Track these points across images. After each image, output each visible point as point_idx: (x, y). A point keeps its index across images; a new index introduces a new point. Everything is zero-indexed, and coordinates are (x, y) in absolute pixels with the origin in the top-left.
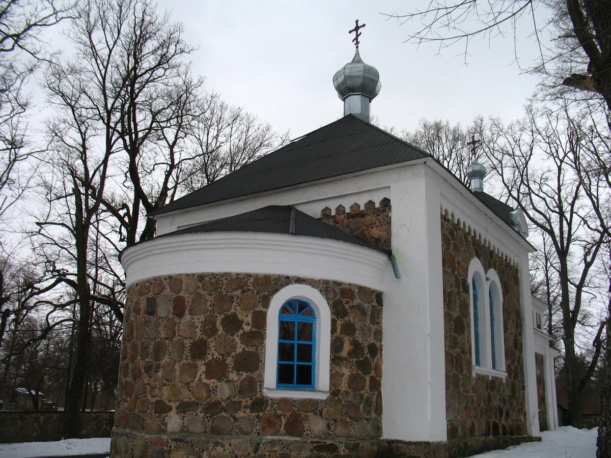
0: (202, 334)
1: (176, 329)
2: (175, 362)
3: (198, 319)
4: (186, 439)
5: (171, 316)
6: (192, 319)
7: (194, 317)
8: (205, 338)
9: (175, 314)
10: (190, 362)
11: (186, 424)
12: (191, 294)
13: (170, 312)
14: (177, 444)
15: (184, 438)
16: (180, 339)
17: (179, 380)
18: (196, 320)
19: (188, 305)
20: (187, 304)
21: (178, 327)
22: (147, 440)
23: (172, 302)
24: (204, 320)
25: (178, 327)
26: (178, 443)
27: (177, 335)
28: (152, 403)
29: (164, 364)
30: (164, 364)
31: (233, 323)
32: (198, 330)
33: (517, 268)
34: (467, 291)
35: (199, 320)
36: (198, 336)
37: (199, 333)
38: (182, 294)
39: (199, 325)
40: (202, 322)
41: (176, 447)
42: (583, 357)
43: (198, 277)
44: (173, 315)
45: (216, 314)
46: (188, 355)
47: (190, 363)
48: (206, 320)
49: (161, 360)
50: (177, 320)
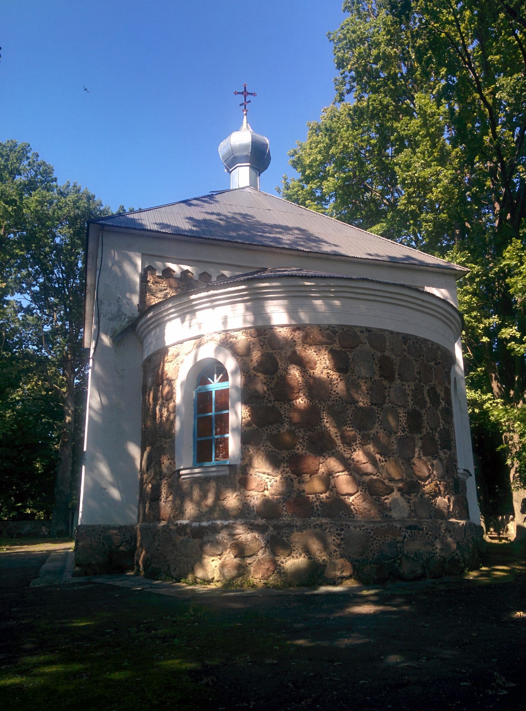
0: (413, 404)
1: (386, 394)
2: (391, 434)
3: (409, 386)
4: (421, 525)
5: (377, 378)
6: (403, 385)
7: (404, 383)
8: (418, 408)
9: (383, 377)
10: (408, 435)
11: (413, 508)
12: (397, 356)
13: (375, 373)
14: (411, 533)
15: (419, 525)
16: (393, 407)
17: (398, 455)
18: (407, 387)
19: (396, 367)
20: (395, 366)
21: (389, 391)
22: (369, 531)
23: (377, 362)
24: (414, 388)
25: (389, 391)
26: (413, 531)
27: (387, 401)
28: (364, 483)
29: (374, 434)
30: (374, 434)
31: (432, 392)
32: (409, 399)
33: (162, 322)
34: (450, 383)
35: (409, 387)
36: (410, 406)
37: (411, 403)
38: (387, 353)
39: (410, 393)
40: (412, 390)
41: (412, 536)
42: (203, 566)
43: (403, 338)
44: (380, 377)
45: (422, 384)
46: (405, 426)
47: (407, 436)
48: (416, 389)
49: (371, 429)
50: (385, 383)
